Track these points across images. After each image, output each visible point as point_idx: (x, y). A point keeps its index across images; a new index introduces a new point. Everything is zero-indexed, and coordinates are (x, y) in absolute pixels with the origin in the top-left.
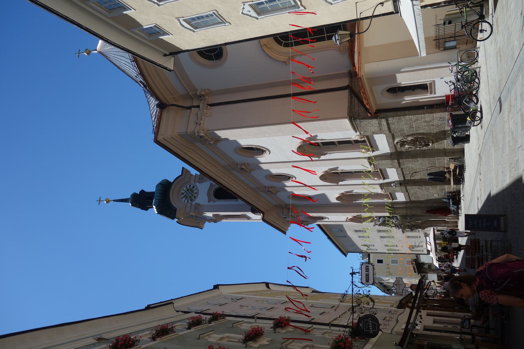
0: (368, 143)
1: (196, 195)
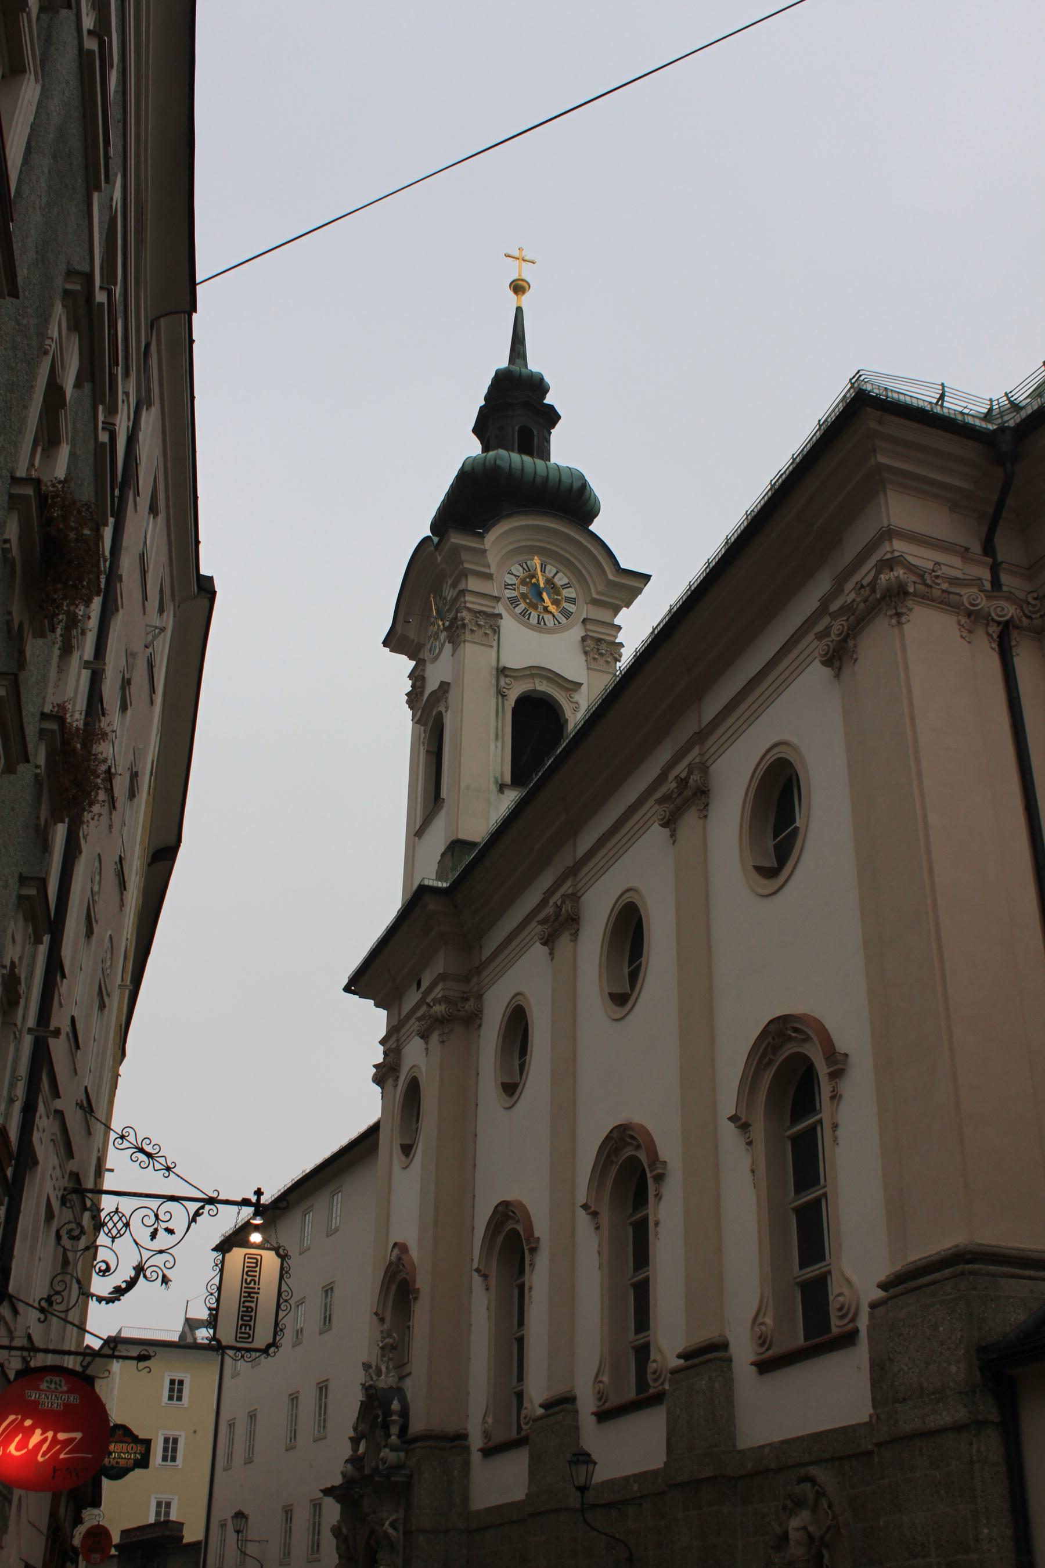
0: (814, 1326)
1: (534, 620)
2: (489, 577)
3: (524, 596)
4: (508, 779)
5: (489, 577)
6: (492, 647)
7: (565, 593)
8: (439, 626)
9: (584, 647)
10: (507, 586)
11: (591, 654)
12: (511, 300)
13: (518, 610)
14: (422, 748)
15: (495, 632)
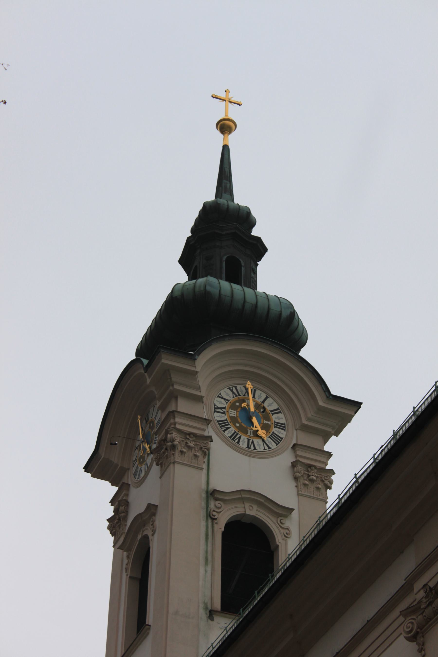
2: (199, 399)
3: (234, 420)
4: (218, 605)
5: (199, 399)
6: (202, 469)
7: (275, 418)
8: (145, 449)
9: (294, 473)
10: (216, 409)
11: (302, 480)
12: (218, 139)
13: (228, 434)
14: (124, 574)
15: (205, 454)
